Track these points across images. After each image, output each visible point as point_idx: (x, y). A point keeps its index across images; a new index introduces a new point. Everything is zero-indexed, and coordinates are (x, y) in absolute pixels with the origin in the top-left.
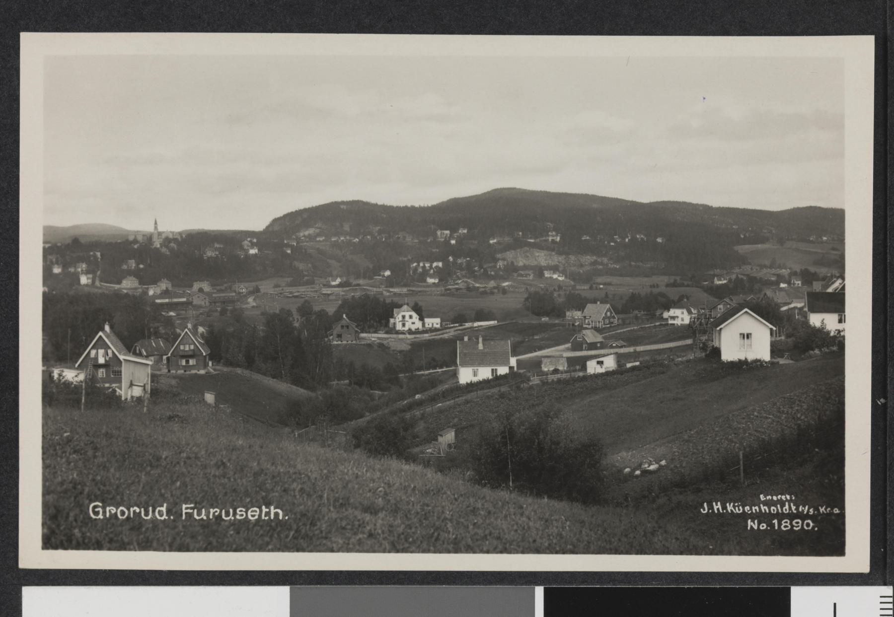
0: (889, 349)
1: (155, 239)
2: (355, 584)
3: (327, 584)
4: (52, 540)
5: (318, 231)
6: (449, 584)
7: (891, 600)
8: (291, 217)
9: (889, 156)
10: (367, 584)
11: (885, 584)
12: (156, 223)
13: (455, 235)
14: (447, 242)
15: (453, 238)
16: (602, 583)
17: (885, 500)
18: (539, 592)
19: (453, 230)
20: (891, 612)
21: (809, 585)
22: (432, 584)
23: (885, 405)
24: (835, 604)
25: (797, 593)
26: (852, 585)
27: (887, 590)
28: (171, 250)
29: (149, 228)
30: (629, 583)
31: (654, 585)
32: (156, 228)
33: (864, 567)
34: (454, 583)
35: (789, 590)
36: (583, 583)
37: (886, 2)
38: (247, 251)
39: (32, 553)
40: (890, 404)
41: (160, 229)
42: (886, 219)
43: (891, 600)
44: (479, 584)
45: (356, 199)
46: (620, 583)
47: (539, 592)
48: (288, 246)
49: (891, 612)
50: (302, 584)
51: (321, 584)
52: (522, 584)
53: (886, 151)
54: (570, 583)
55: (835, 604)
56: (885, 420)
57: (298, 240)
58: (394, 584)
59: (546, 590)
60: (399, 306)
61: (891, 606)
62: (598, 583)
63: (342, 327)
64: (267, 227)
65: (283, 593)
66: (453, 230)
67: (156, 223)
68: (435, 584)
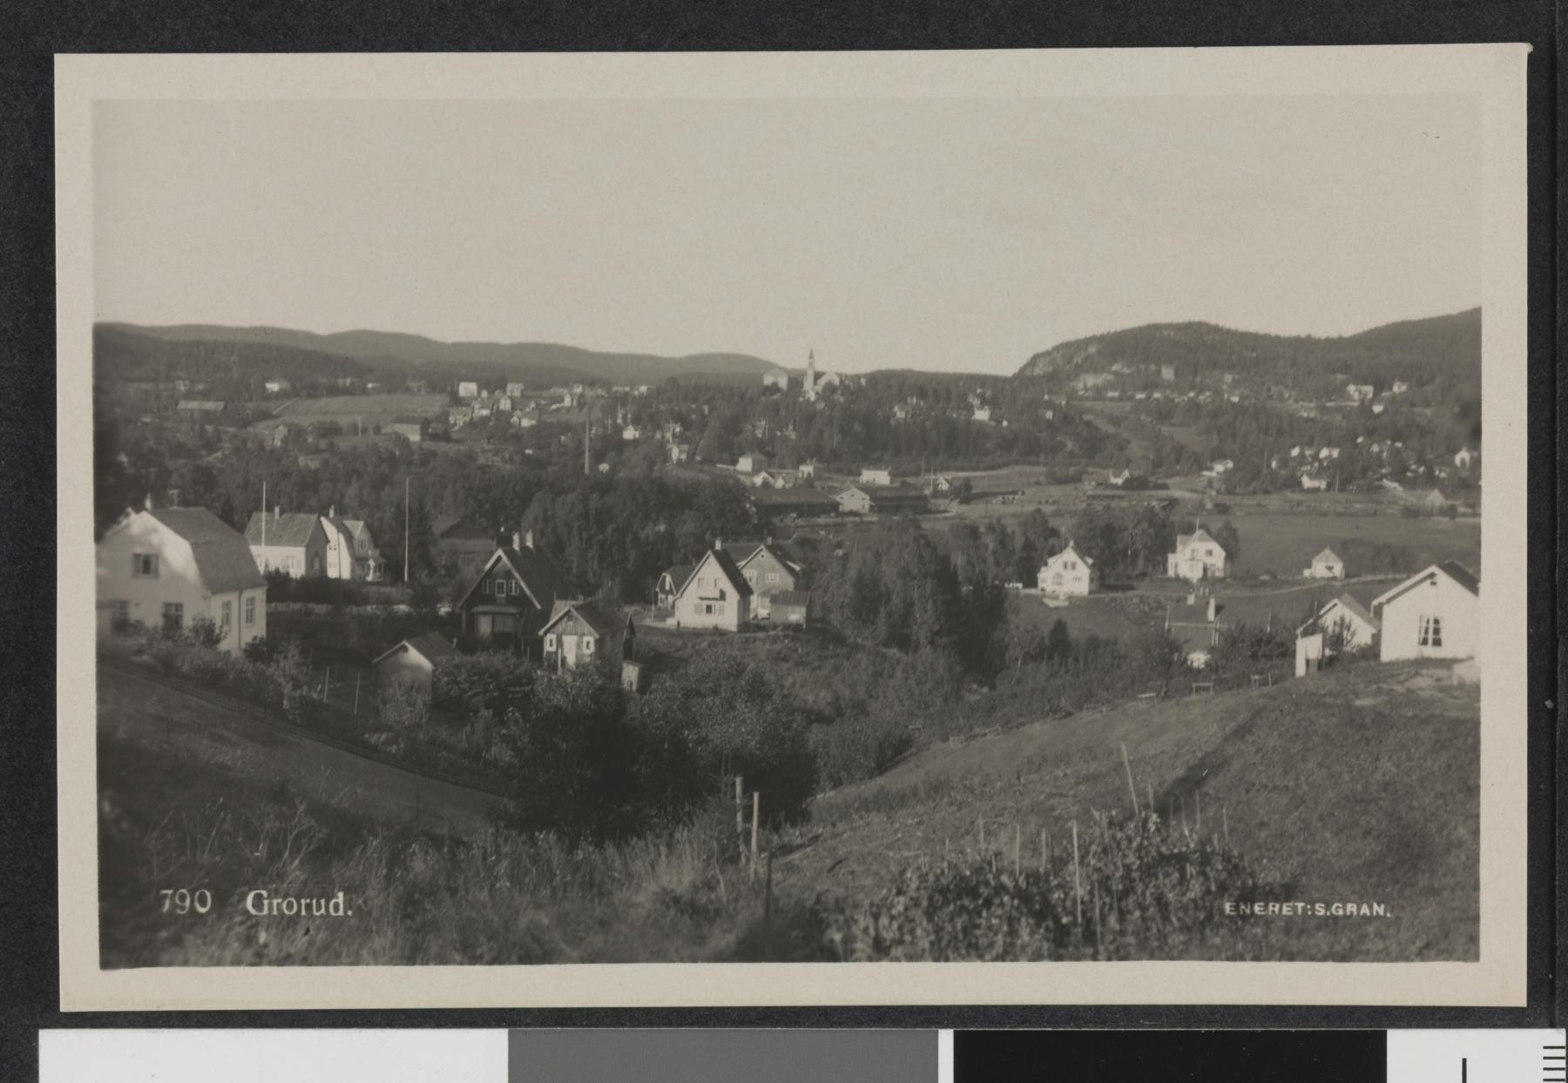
0: (1559, 613)
1: (808, 384)
2: (623, 1025)
3: (574, 1025)
4: (120, 947)
5: (1110, 377)
6: (786, 1025)
7: (1563, 1053)
8: (1069, 349)
9: (1559, 274)
10: (644, 1025)
11: (1552, 1025)
12: (811, 356)
13: (1386, 394)
14: (1365, 408)
15: (1381, 401)
16: (1055, 1024)
17: (1553, 878)
18: (946, 1039)
19: (1381, 385)
20: (1562, 1075)
21: (1418, 1027)
22: (758, 1025)
23: (1553, 713)
24: (1464, 1061)
25: (1399, 1042)
26: (1495, 1026)
27: (1556, 1036)
28: (832, 406)
29: (797, 362)
30: (1104, 1023)
31: (1146, 1027)
32: (811, 365)
33: (1516, 995)
34: (797, 1024)
35: (1384, 1035)
36: (1022, 1023)
37: (1553, 4)
38: (970, 409)
39: (81, 975)
40: (1561, 709)
41: (819, 367)
42: (1553, 385)
43: (1563, 1053)
44: (840, 1024)
45: (1195, 318)
46: (1087, 1023)
47: (946, 1038)
48: (1051, 405)
49: (1562, 1075)
50: (529, 1025)
51: (562, 1025)
52: (916, 1026)
53: (1554, 264)
54: (1001, 1023)
55: (1464, 1061)
56: (1553, 738)
57: (1072, 395)
58: (691, 1025)
59: (957, 1036)
60: (1189, 530)
61: (1562, 1064)
62: (1049, 1023)
63: (1065, 566)
64: (1023, 370)
65: (497, 1040)
66: (1381, 385)
67: (811, 356)
68: (764, 1025)
